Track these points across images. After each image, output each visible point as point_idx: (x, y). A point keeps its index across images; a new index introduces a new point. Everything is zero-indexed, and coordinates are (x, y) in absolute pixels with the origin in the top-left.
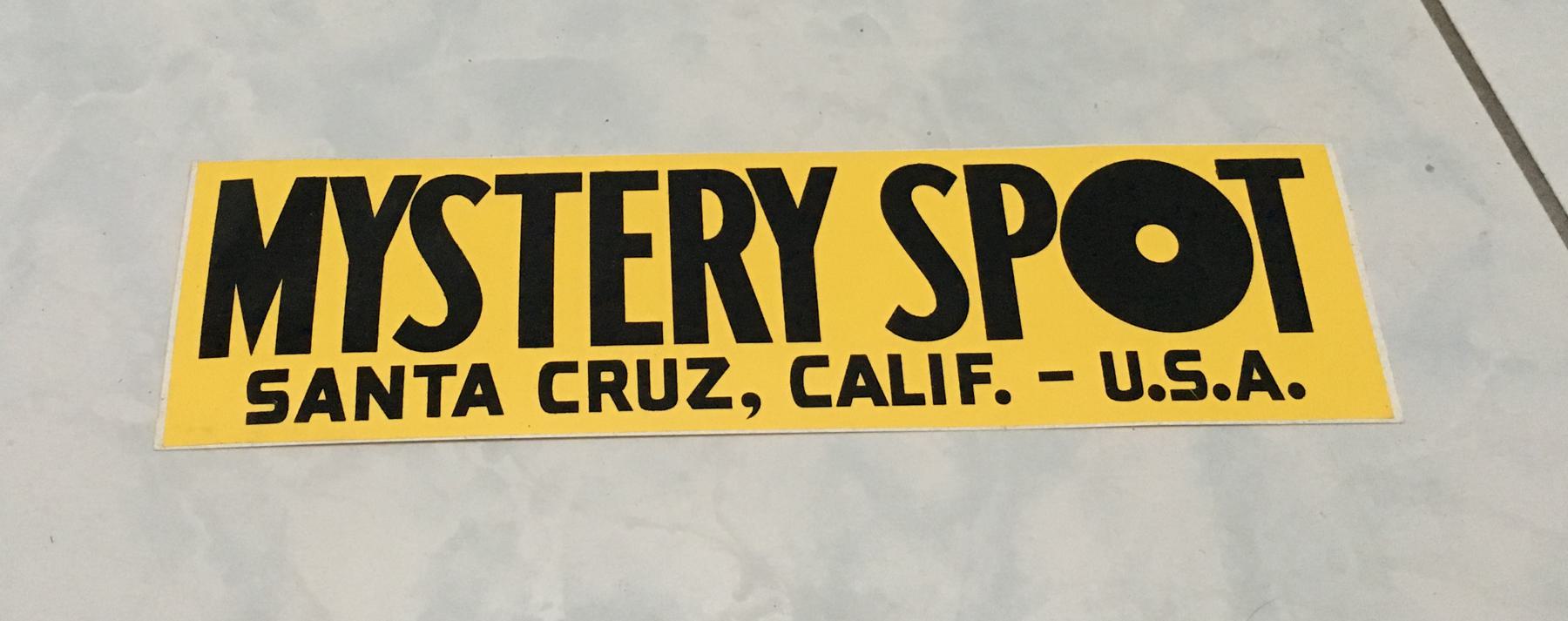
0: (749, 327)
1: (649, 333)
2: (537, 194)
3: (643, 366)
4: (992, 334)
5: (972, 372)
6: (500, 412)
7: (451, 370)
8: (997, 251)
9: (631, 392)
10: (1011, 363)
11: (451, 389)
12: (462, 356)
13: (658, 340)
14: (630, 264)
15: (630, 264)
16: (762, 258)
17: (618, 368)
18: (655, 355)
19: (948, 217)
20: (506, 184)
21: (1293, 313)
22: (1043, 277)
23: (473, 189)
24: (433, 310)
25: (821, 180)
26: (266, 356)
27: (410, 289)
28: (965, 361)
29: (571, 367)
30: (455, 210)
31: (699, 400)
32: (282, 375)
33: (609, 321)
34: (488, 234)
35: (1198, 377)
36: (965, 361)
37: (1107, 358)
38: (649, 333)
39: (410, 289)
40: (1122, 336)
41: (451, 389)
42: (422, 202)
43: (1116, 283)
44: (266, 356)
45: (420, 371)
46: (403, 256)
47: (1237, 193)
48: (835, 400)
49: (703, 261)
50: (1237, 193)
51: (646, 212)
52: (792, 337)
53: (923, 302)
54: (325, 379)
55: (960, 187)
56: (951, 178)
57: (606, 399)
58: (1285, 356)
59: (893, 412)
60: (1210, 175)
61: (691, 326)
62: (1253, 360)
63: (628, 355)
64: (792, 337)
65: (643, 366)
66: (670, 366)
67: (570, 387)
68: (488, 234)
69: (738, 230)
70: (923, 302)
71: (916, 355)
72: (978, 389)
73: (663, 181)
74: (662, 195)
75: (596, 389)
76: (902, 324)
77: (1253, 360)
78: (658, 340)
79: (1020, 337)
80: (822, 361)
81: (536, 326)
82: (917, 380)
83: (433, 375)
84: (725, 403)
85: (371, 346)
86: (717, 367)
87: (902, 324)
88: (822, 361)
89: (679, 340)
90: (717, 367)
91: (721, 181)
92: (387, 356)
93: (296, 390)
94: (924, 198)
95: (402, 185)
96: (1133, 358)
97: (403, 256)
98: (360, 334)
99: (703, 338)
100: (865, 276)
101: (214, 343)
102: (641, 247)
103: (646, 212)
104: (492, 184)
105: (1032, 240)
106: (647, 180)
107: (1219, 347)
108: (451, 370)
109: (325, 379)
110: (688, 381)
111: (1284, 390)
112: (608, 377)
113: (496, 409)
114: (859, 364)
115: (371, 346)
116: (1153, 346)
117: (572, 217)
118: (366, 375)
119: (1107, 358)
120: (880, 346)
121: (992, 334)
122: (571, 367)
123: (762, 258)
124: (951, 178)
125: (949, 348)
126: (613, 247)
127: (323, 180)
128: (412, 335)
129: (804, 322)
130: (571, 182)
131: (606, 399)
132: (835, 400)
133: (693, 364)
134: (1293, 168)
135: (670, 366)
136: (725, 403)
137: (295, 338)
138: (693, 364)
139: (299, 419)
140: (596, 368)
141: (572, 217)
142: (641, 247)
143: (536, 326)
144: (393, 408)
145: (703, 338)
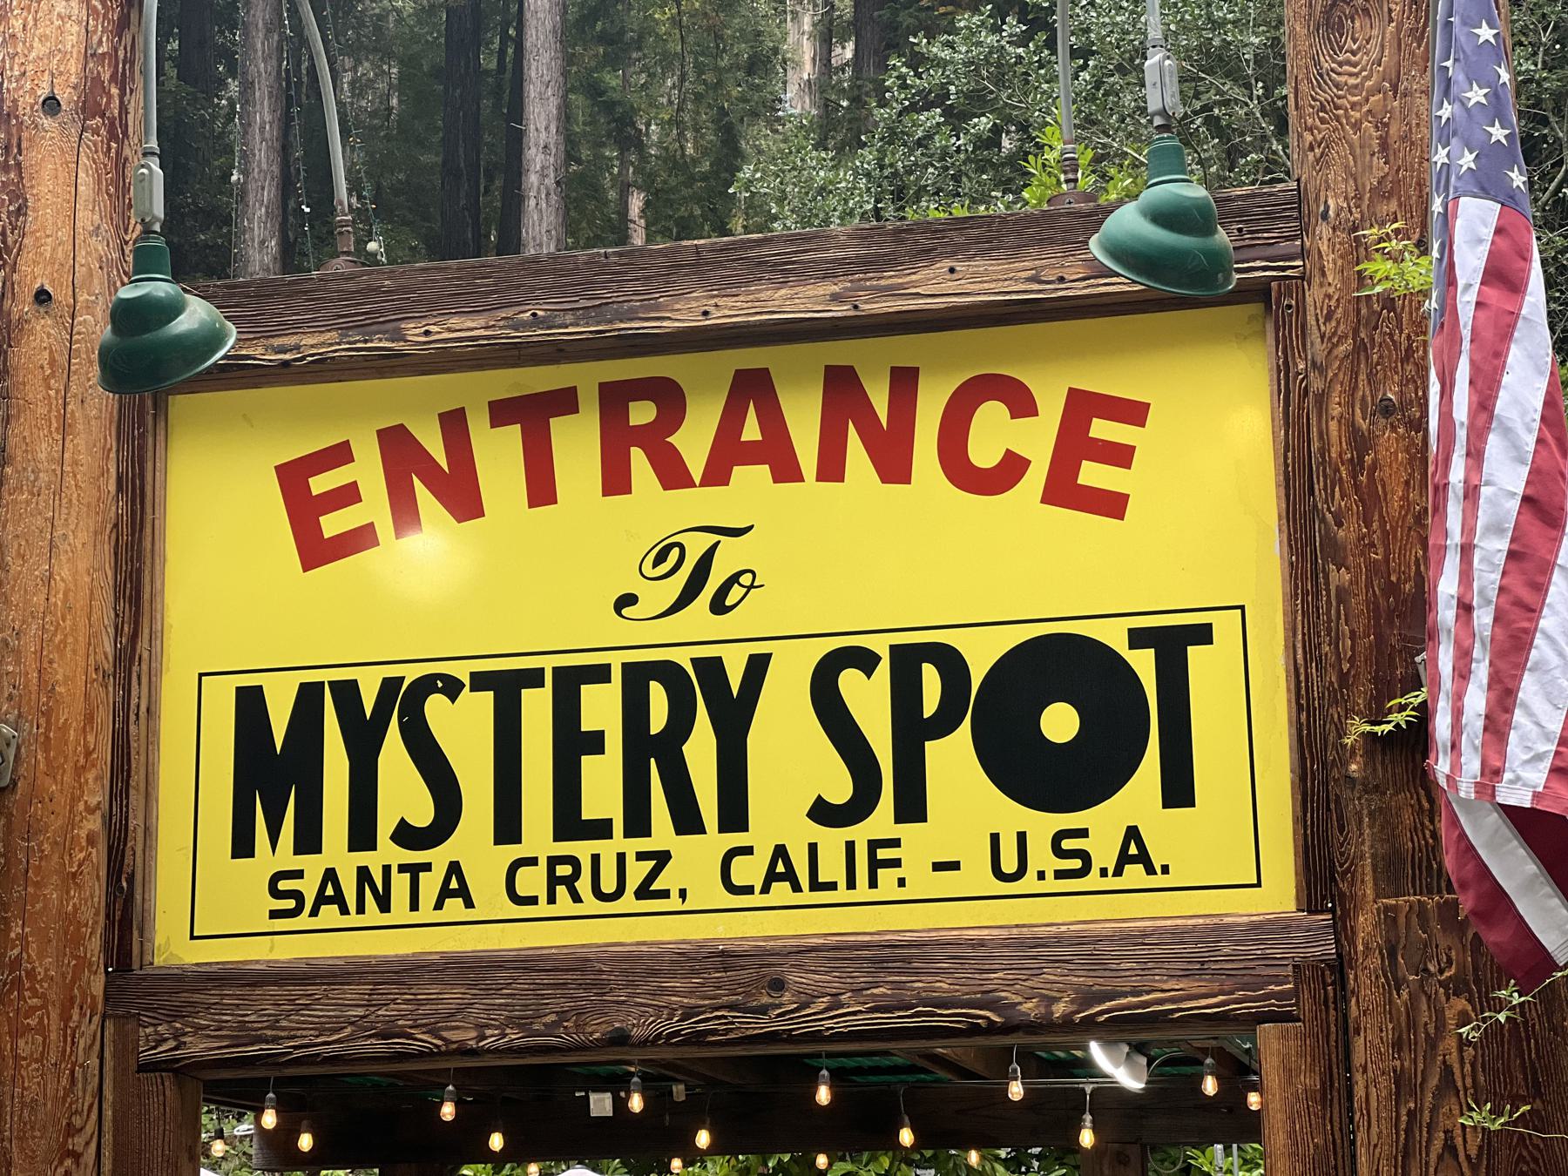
0: (687, 820)
1: (602, 829)
2: (507, 689)
3: (596, 859)
4: (900, 818)
5: (880, 857)
6: (473, 906)
7: (427, 867)
8: (913, 732)
9: (584, 885)
10: (918, 844)
11: (430, 884)
12: (439, 857)
13: (608, 834)
14: (586, 760)
15: (586, 760)
16: (701, 752)
17: (573, 861)
18: (607, 849)
19: (869, 700)
20: (480, 681)
21: (1178, 789)
22: (953, 760)
23: (452, 688)
24: (422, 813)
25: (758, 667)
26: (286, 857)
27: (403, 793)
28: (874, 845)
29: (533, 861)
30: (436, 707)
31: (644, 892)
32: (298, 874)
33: (570, 821)
34: (464, 728)
35: (1084, 856)
36: (874, 845)
37: (995, 839)
38: (602, 829)
39: (403, 793)
40: (1012, 816)
41: (430, 884)
42: (406, 702)
43: (1022, 769)
44: (286, 857)
45: (403, 868)
46: (394, 755)
47: (1143, 663)
48: (757, 889)
49: (654, 754)
50: (1143, 663)
51: (601, 708)
52: (724, 828)
53: (840, 790)
54: (330, 875)
55: (883, 670)
56: (876, 659)
57: (561, 890)
58: (1166, 832)
59: (807, 897)
60: (1119, 644)
61: (638, 823)
62: (1133, 833)
63: (582, 849)
64: (724, 828)
65: (596, 859)
66: (621, 858)
67: (532, 881)
68: (464, 728)
69: (681, 723)
70: (840, 790)
71: (832, 841)
72: (882, 873)
73: (616, 674)
74: (615, 687)
75: (553, 881)
76: (823, 813)
77: (1133, 833)
78: (608, 834)
79: (496, 843)
80: (748, 851)
81: (508, 827)
82: (830, 868)
83: (414, 871)
84: (665, 894)
85: (371, 845)
86: (662, 858)
87: (823, 813)
88: (748, 851)
89: (628, 833)
90: (662, 858)
91: (668, 673)
92: (388, 853)
93: (309, 888)
94: (850, 681)
95: (390, 687)
96: (1022, 837)
97: (394, 755)
98: (362, 835)
99: (647, 833)
100: (792, 761)
101: (243, 846)
102: (595, 743)
103: (601, 708)
104: (467, 681)
105: (943, 725)
106: (600, 674)
107: (1103, 825)
108: (427, 867)
109: (330, 875)
110: (637, 872)
111: (1159, 870)
112: (564, 870)
113: (469, 904)
114: (780, 852)
115: (371, 845)
116: (1042, 825)
117: (537, 706)
118: (364, 874)
119: (995, 839)
120: (799, 834)
121: (900, 818)
122: (533, 861)
123: (701, 752)
124: (876, 659)
125: (861, 833)
126: (573, 743)
127: (705, 482)
128: (405, 835)
129: (734, 815)
130: (533, 678)
131: (561, 890)
132: (757, 889)
133: (641, 856)
134: (1203, 634)
135: (621, 858)
136: (665, 894)
137: (309, 841)
138: (641, 856)
139: (311, 915)
140: (553, 862)
141: (537, 706)
142: (595, 743)
143: (508, 827)
144: (464, 500)
145: (647, 833)
